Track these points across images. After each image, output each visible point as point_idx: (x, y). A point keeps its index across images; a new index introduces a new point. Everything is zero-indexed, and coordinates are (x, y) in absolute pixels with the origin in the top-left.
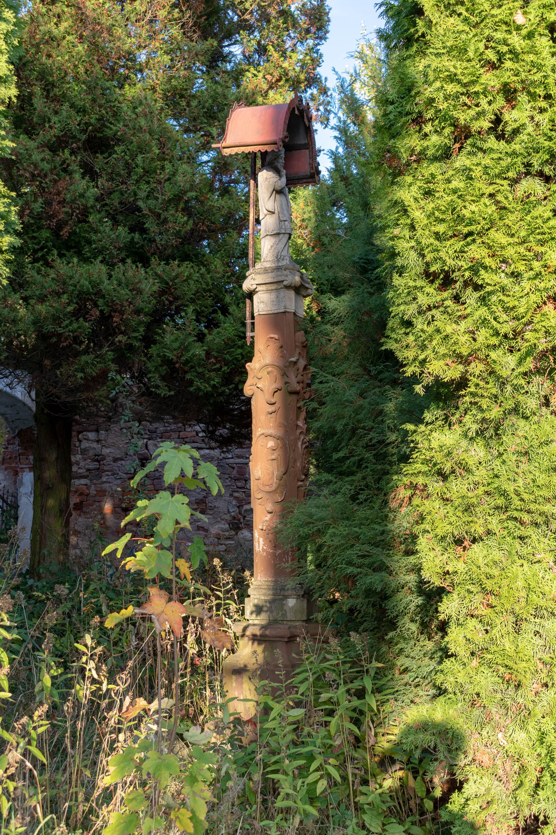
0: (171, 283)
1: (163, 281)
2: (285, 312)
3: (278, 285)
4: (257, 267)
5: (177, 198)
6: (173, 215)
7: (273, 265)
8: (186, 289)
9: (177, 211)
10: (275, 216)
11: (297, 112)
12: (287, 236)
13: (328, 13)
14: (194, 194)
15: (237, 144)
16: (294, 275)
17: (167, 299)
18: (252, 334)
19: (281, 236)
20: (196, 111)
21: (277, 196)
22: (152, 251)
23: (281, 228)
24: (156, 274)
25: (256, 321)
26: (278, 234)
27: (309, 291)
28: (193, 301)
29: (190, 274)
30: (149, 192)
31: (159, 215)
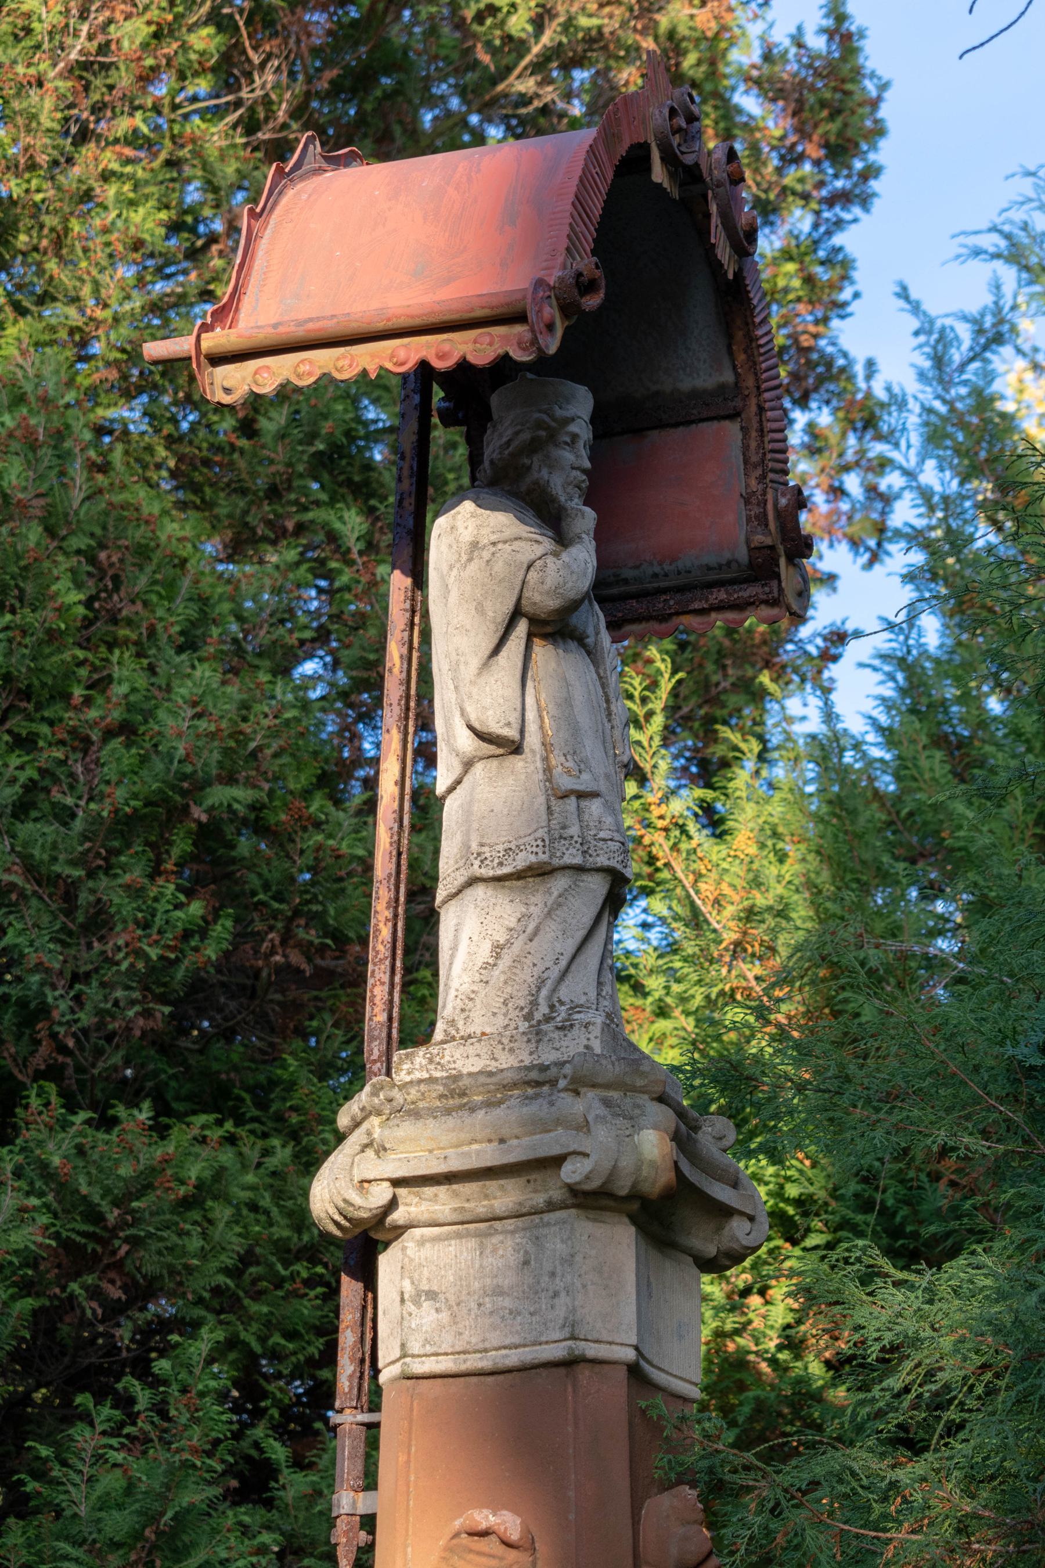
0: (112, 1216)
1: (68, 1200)
2: (570, 1363)
3: (545, 1187)
4: (401, 1076)
5: (155, 818)
6: (135, 892)
7: (506, 1061)
8: (195, 1243)
9: (155, 872)
10: (524, 769)
11: (659, 174)
12: (597, 887)
13: (875, 104)
14: (240, 795)
15: (299, 332)
16: (635, 1123)
17: (94, 1293)
18: (363, 1503)
19: (560, 883)
20: (281, 454)
21: (542, 651)
22: (38, 1061)
23: (555, 838)
24: (44, 1167)
25: (390, 1418)
26: (540, 872)
27: (738, 1227)
28: (223, 1302)
29: (220, 1173)
30: (31, 787)
31: (69, 894)
